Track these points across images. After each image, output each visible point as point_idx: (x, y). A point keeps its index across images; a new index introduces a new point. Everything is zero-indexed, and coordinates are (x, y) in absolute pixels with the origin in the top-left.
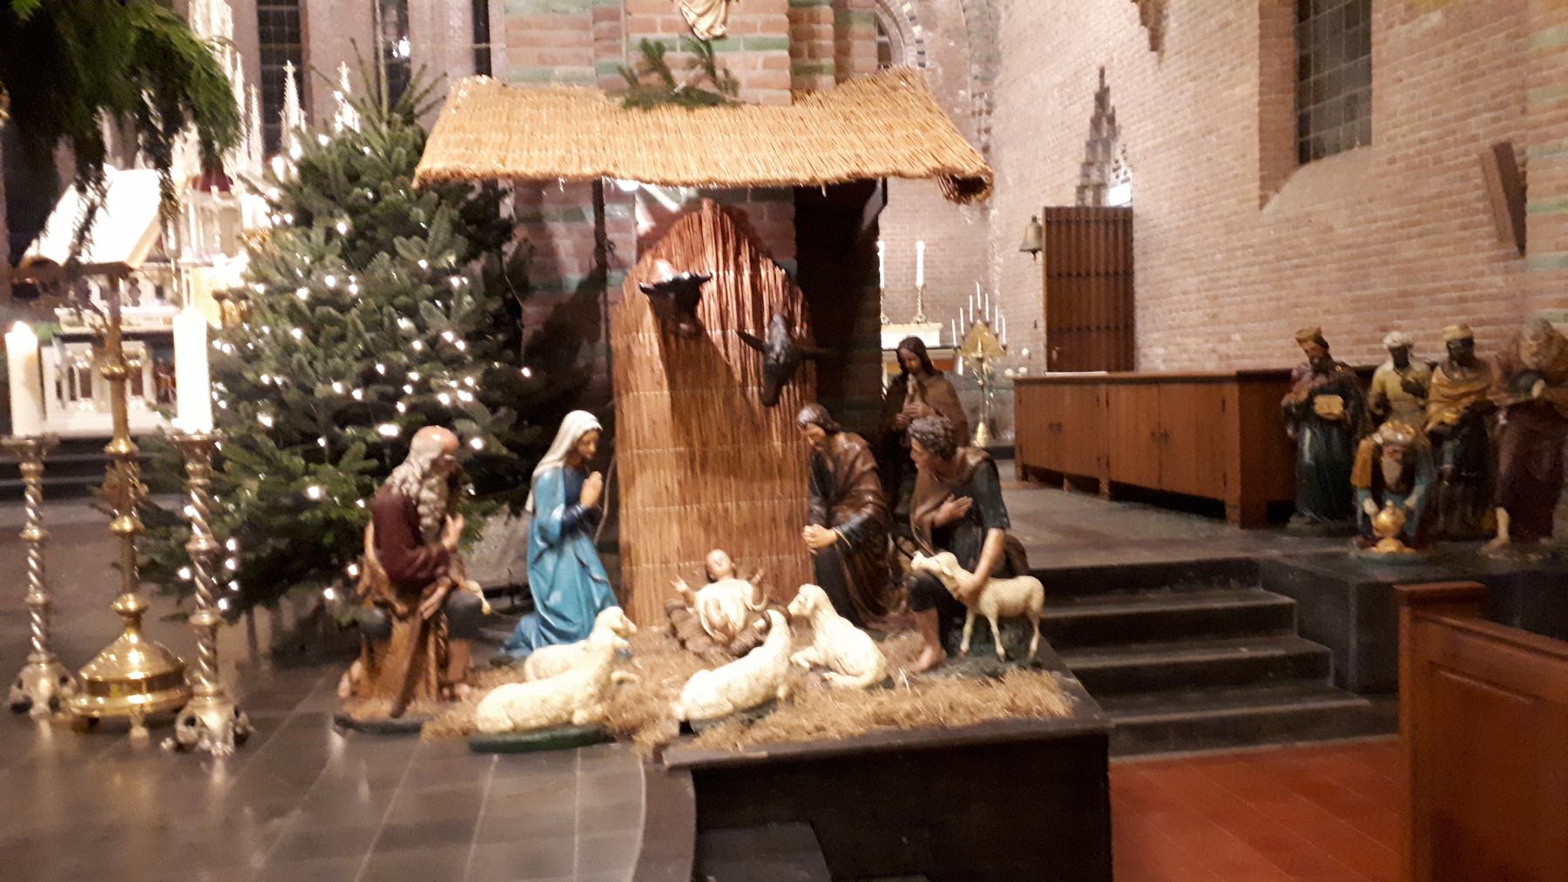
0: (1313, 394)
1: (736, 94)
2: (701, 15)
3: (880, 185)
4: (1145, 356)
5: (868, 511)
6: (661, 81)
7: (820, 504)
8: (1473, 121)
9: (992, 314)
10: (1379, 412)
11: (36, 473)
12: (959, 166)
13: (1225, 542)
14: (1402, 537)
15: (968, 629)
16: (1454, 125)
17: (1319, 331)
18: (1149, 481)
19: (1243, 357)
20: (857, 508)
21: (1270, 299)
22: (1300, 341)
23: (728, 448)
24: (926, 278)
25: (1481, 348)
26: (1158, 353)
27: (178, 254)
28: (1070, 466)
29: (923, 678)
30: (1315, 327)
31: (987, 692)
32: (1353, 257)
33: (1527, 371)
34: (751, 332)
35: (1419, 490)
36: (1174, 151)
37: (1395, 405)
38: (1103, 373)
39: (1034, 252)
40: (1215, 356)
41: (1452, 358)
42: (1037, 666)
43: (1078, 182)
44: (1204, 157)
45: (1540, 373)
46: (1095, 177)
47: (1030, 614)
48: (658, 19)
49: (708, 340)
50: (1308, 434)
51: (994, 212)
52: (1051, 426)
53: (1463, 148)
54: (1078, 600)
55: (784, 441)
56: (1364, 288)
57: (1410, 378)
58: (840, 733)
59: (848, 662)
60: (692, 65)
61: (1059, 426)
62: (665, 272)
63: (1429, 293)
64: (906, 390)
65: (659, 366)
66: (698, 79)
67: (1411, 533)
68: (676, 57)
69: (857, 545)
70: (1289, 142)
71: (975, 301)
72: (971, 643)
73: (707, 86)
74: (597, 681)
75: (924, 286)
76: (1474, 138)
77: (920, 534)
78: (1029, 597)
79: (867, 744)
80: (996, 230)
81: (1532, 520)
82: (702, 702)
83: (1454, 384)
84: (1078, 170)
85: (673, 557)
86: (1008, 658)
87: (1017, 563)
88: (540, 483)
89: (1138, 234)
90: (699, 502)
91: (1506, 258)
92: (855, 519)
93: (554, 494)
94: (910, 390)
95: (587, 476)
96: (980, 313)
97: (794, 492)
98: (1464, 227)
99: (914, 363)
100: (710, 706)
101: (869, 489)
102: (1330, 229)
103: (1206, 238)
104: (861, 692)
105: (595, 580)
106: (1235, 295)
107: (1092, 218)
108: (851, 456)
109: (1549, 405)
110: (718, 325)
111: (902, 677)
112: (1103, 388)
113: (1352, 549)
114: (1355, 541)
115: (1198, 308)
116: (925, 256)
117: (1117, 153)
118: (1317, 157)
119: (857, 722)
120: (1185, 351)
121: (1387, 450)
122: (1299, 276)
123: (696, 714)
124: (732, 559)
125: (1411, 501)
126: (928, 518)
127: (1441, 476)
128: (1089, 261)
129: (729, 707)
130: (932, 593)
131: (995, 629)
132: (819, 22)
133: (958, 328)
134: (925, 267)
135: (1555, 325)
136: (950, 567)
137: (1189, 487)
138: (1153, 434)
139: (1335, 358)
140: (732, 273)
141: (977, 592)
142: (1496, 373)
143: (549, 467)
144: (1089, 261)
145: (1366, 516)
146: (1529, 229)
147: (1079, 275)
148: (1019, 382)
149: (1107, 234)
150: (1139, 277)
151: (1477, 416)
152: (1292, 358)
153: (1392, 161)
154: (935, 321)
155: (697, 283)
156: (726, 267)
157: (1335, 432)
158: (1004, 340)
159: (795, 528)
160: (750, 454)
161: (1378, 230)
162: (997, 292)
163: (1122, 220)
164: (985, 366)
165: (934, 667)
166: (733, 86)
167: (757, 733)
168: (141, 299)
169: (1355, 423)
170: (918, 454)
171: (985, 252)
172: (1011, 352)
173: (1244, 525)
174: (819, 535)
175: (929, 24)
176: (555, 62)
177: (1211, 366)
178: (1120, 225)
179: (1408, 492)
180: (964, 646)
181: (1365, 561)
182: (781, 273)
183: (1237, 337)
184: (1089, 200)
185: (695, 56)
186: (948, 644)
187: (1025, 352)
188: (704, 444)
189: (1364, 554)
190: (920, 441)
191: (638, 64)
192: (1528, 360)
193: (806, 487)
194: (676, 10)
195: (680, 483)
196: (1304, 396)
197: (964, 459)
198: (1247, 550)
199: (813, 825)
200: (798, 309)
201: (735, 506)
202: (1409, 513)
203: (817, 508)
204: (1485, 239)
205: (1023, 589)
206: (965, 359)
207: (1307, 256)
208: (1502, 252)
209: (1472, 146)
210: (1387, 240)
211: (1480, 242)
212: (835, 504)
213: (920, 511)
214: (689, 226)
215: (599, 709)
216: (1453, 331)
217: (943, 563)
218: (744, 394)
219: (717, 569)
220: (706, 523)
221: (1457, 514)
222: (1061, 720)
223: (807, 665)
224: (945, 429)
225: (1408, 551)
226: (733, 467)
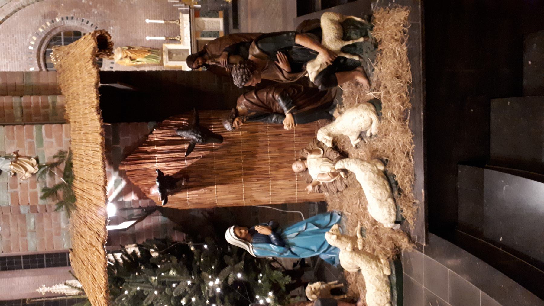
1: (67, 152)
2: (26, 170)
5: (277, 96)
6: (62, 193)
12: (91, 50)
15: (347, 56)
20: (274, 101)
23: (242, 158)
24: (161, 19)
29: (374, 85)
34: (186, 146)
42: (370, 18)
47: (341, 21)
48: (30, 190)
49: (190, 167)
60: (52, 175)
62: (155, 191)
64: (214, 65)
65: (202, 191)
66: (59, 171)
68: (49, 182)
69: (294, 104)
72: (355, 54)
73: (62, 167)
74: (369, 262)
75: (164, 20)
77: (295, 78)
78: (332, 21)
82: (387, 216)
85: (293, 183)
86: (366, 36)
87: (314, 26)
88: (258, 255)
90: (267, 171)
93: (265, 249)
94: (214, 63)
95: (257, 232)
97: (264, 129)
100: (390, 211)
105: (306, 228)
108: (248, 104)
110: (183, 162)
111: (371, 95)
123: (393, 218)
124: (297, 160)
126: (286, 75)
129: (390, 200)
130: (329, 75)
131: (350, 42)
132: (31, 103)
136: (314, 67)
140: (156, 155)
141: (329, 52)
143: (253, 250)
154: (178, 15)
155: (161, 177)
156: (153, 158)
160: (244, 147)
165: (367, 76)
166: (61, 154)
167: (407, 190)
175: (55, 15)
176: (60, 228)
180: (356, 58)
182: (155, 131)
185: (48, 172)
186: (352, 67)
188: (240, 168)
190: (245, 83)
191: (54, 200)
194: (25, 182)
195: (258, 180)
197: (254, 55)
200: (173, 122)
201: (269, 155)
212: (272, 111)
213: (282, 78)
214: (132, 176)
217: (312, 71)
218: (216, 150)
219: (302, 168)
220: (277, 168)
223: (359, 140)
224: (240, 68)
226: (252, 154)
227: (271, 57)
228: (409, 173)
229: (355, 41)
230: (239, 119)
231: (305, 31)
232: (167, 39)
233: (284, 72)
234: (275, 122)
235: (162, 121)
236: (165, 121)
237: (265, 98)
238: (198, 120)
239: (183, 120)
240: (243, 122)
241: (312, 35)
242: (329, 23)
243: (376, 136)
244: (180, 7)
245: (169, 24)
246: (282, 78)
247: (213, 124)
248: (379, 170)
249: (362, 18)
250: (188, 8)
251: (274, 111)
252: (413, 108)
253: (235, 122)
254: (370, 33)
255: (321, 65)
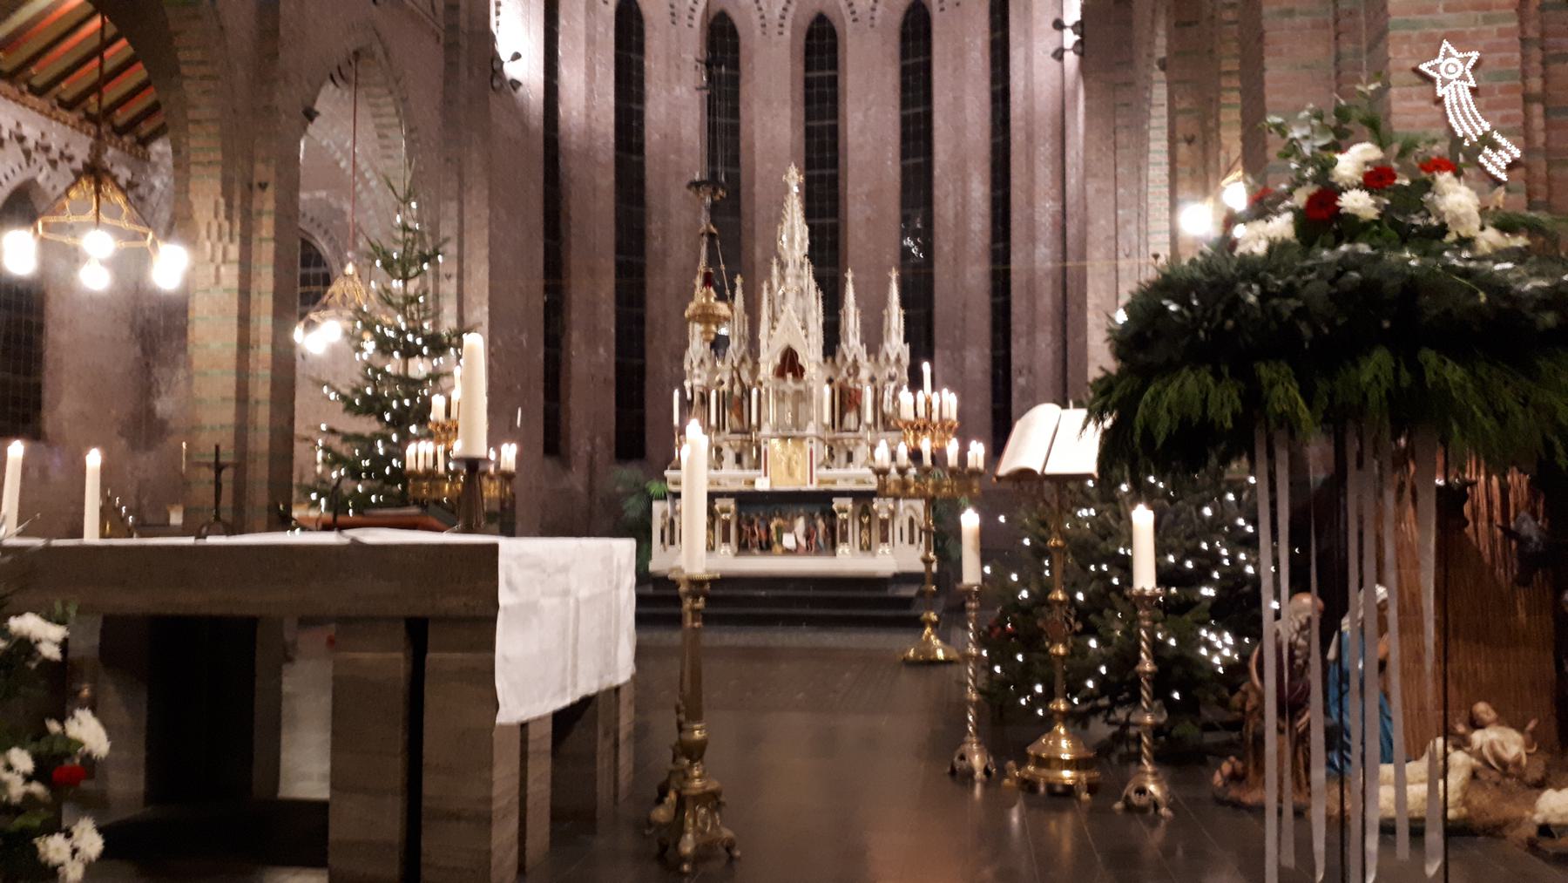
11: (976, 610)
27: (759, 427)
55: (1528, 615)
168: (724, 463)
200: (1540, 507)
215: (1464, 810)
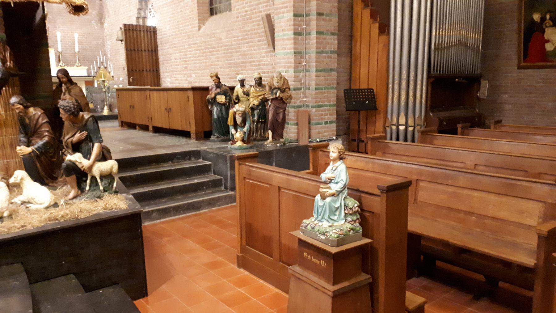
0: (216, 95)
3: (41, 5)
4: (164, 81)
5: (46, 139)
7: (24, 137)
8: (260, 6)
9: (107, 64)
10: (237, 101)
13: (191, 145)
14: (243, 141)
15: (88, 182)
16: (255, 7)
17: (217, 74)
18: (165, 126)
19: (196, 82)
20: (41, 138)
21: (203, 63)
22: (211, 77)
24: (79, 49)
25: (264, 81)
26: (169, 79)
28: (138, 121)
29: (71, 201)
30: (216, 72)
31: (96, 204)
32: (228, 49)
33: (275, 88)
35: (247, 125)
36: (169, 7)
37: (241, 99)
38: (149, 87)
39: (122, 41)
40: (187, 82)
41: (256, 83)
42: (116, 192)
43: (136, 15)
44: (179, 10)
45: (279, 89)
46: (143, 14)
47: (112, 174)
50: (215, 108)
51: (106, 25)
52: (130, 106)
53: (258, 14)
54: (139, 168)
56: (231, 60)
57: (245, 90)
58: (33, 226)
59: (37, 200)
61: (133, 107)
63: (250, 62)
67: (245, 139)
69: (41, 153)
70: (207, 8)
71: (100, 59)
72: (90, 186)
75: (79, 52)
76: (261, 12)
78: (112, 168)
79: (43, 229)
80: (107, 32)
81: (278, 134)
83: (257, 92)
84: (135, 11)
86: (105, 191)
87: (107, 155)
89: (159, 37)
91: (270, 52)
92: (40, 143)
94: (64, 91)
96: (102, 63)
97: (10, 133)
98: (259, 41)
99: (64, 80)
101: (46, 130)
102: (221, 39)
103: (182, 40)
104: (43, 210)
106: (192, 61)
107: (142, 29)
108: (36, 117)
109: (282, 99)
111: (62, 202)
112: (148, 92)
113: (229, 145)
114: (230, 143)
115: (181, 65)
116: (79, 40)
117: (150, 6)
118: (216, 14)
119: (41, 221)
120: (177, 80)
121: (237, 113)
122: (212, 55)
125: (245, 129)
126: (70, 140)
127: (254, 122)
128: (141, 46)
130: (73, 169)
133: (94, 69)
134: (79, 44)
135: (282, 74)
137: (178, 127)
138: (166, 109)
139: (222, 83)
141: (91, 167)
142: (267, 88)
144: (141, 46)
145: (232, 135)
146: (276, 43)
147: (138, 50)
148: (118, 90)
149: (147, 36)
150: (160, 53)
151: (264, 102)
152: (209, 83)
153: (238, 17)
154: (85, 66)
157: (223, 107)
158: (112, 74)
159: (13, 146)
161: (235, 41)
162: (109, 55)
163: (153, 31)
164: (106, 84)
165: (75, 197)
169: (229, 105)
170: (63, 115)
171: (103, 40)
172: (115, 79)
173: (197, 140)
174: (23, 150)
177: (186, 85)
178: (152, 33)
179: (244, 126)
181: (232, 149)
183: (193, 75)
184: (141, 23)
187: (121, 79)
189: (232, 146)
190: (63, 109)
192: (276, 85)
193: (18, 129)
196: (213, 95)
197: (83, 116)
198: (198, 147)
199: (22, 263)
200: (8, 55)
202: (245, 133)
203: (22, 139)
204: (264, 47)
205: (110, 165)
206: (98, 81)
207: (214, 48)
208: (269, 50)
209: (260, 14)
210: (238, 44)
211: (263, 46)
213: (66, 138)
216: (256, 75)
217: (76, 158)
221: (259, 133)
222: (124, 210)
223: (20, 202)
224: (74, 105)
225: (244, 145)
227: (84, 127)
228: (9, 229)
229: (100, 184)
230: (22, 109)
231: (104, 150)
232: (61, 53)
233: (72, 138)
234: (20, 140)
235: (8, 45)
236: (8, 48)
237: (43, 130)
238: (13, 75)
239: (10, 63)
240: (19, 112)
241: (101, 155)
242: (111, 165)
243: (29, 210)
244: (94, 67)
245: (75, 56)
246: (66, 138)
247: (9, 89)
248: (3, 213)
249: (116, 188)
250: (93, 75)
251: (31, 139)
252: (60, 223)
253: (19, 106)
254: (107, 193)
255: (81, 163)
